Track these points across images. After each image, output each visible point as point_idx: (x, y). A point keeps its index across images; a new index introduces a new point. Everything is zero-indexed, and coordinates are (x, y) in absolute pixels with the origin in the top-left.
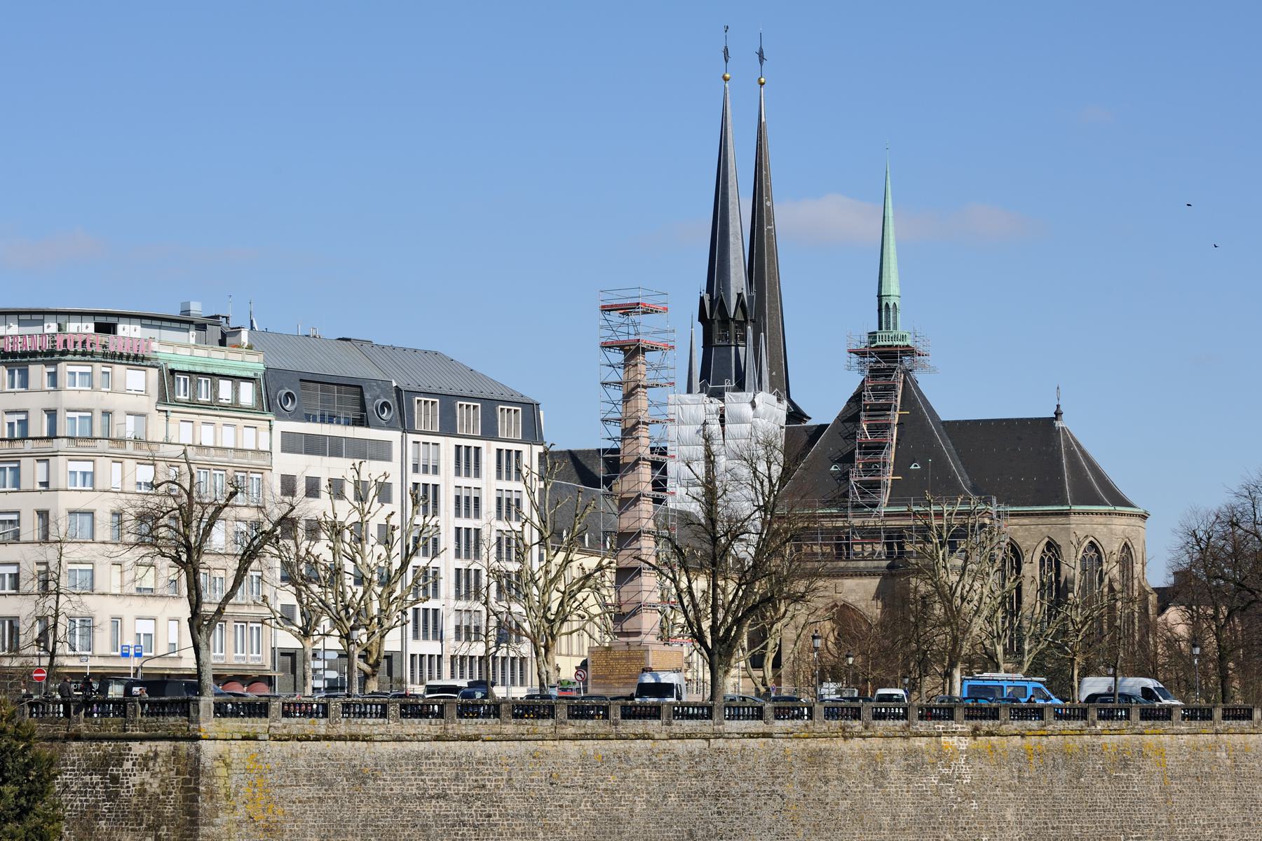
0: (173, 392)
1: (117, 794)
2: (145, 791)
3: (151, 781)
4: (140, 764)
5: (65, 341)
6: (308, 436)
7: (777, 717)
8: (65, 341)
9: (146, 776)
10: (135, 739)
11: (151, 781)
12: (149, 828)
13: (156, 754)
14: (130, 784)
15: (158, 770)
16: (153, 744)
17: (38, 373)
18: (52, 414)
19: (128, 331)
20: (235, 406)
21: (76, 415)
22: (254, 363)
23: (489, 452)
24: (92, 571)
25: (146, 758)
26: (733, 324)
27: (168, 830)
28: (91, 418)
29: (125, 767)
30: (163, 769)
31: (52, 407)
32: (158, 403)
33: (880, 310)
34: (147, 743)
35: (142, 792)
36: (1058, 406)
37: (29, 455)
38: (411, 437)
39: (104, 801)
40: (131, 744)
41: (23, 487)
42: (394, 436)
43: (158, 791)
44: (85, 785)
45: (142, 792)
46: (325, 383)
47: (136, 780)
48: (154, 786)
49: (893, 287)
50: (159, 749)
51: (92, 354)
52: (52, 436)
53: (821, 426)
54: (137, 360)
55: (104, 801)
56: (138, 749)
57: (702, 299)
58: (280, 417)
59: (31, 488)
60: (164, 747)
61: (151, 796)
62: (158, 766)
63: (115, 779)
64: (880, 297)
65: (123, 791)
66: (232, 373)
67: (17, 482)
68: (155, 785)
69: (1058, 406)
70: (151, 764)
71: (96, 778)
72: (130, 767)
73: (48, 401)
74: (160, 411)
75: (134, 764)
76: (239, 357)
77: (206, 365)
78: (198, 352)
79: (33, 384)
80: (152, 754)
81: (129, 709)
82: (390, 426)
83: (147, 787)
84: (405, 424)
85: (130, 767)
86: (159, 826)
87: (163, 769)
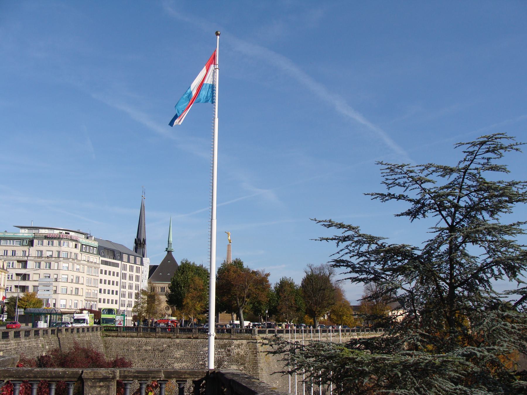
0: (82, 250)
1: (230, 355)
2: (239, 354)
3: (241, 351)
4: (237, 347)
5: (63, 235)
6: (106, 261)
7: (335, 332)
8: (63, 235)
9: (239, 350)
10: (235, 339)
11: (241, 351)
12: (241, 364)
13: (242, 344)
14: (234, 352)
15: (243, 348)
16: (241, 341)
17: (56, 242)
18: (59, 252)
19: (72, 234)
20: (93, 253)
21: (64, 252)
22: (96, 244)
24: (67, 289)
25: (239, 345)
26: (142, 245)
27: (248, 365)
28: (68, 253)
29: (232, 347)
30: (245, 348)
31: (59, 250)
33: (168, 244)
34: (239, 340)
35: (238, 354)
37: (53, 261)
38: (123, 263)
39: (226, 356)
40: (233, 341)
41: (51, 268)
42: (119, 262)
43: (244, 354)
44: (219, 352)
45: (238, 354)
46: (108, 250)
47: (236, 351)
48: (242, 353)
49: (171, 239)
50: (243, 342)
51: (68, 239)
52: (59, 257)
53: (155, 266)
54: (72, 240)
55: (226, 356)
56: (236, 342)
57: (136, 239)
58: (102, 256)
59: (43, 268)
60: (245, 342)
61: (241, 355)
62: (243, 347)
63: (229, 351)
64: (168, 241)
65: (232, 354)
66: (93, 246)
67: (50, 267)
68: (242, 352)
70: (240, 347)
71: (223, 350)
72: (234, 347)
73: (58, 249)
75: (235, 346)
76: (91, 242)
77: (88, 244)
78: (84, 240)
79: (54, 245)
80: (241, 344)
81: (232, 331)
82: (119, 260)
83: (240, 353)
84: (121, 259)
85: (234, 347)
86: (245, 363)
87: (245, 348)
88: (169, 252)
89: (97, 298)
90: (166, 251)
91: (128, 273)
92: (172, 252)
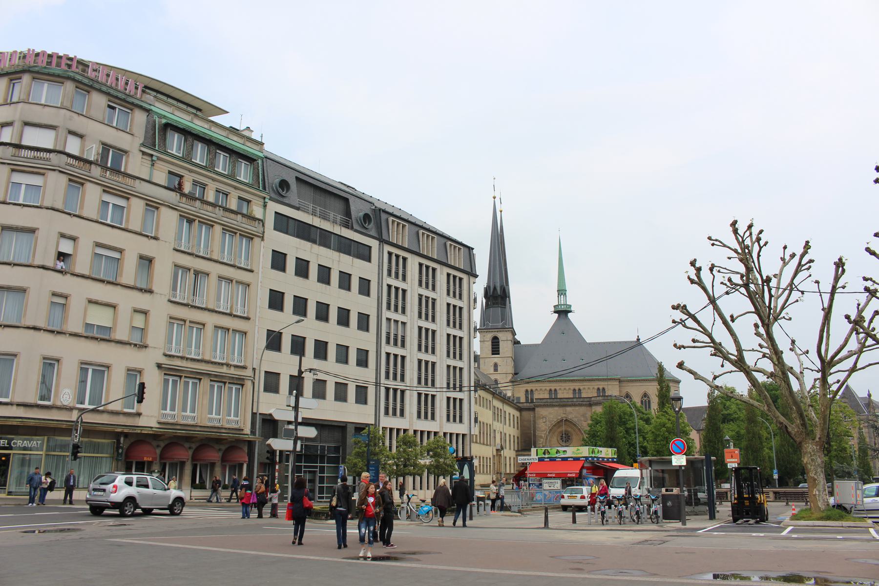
23: (442, 273)
32: (143, 145)
36: (638, 336)
38: (387, 248)
69: (638, 336)
74: (144, 153)
88: (563, 312)
89: (244, 368)
90: (555, 312)
91: (413, 288)
92: (569, 314)
